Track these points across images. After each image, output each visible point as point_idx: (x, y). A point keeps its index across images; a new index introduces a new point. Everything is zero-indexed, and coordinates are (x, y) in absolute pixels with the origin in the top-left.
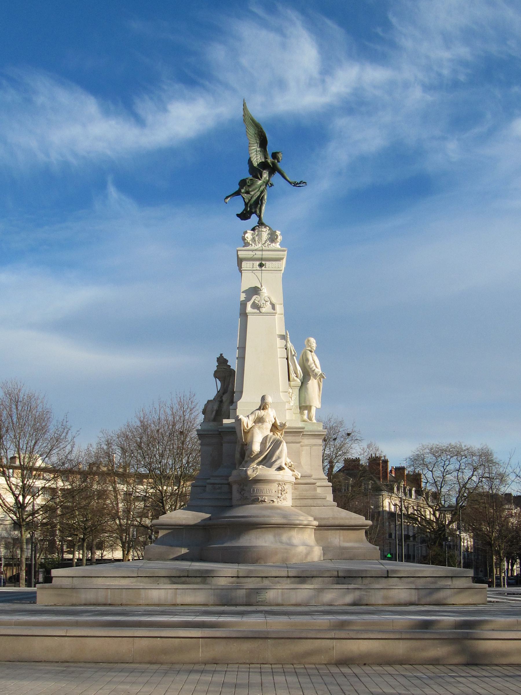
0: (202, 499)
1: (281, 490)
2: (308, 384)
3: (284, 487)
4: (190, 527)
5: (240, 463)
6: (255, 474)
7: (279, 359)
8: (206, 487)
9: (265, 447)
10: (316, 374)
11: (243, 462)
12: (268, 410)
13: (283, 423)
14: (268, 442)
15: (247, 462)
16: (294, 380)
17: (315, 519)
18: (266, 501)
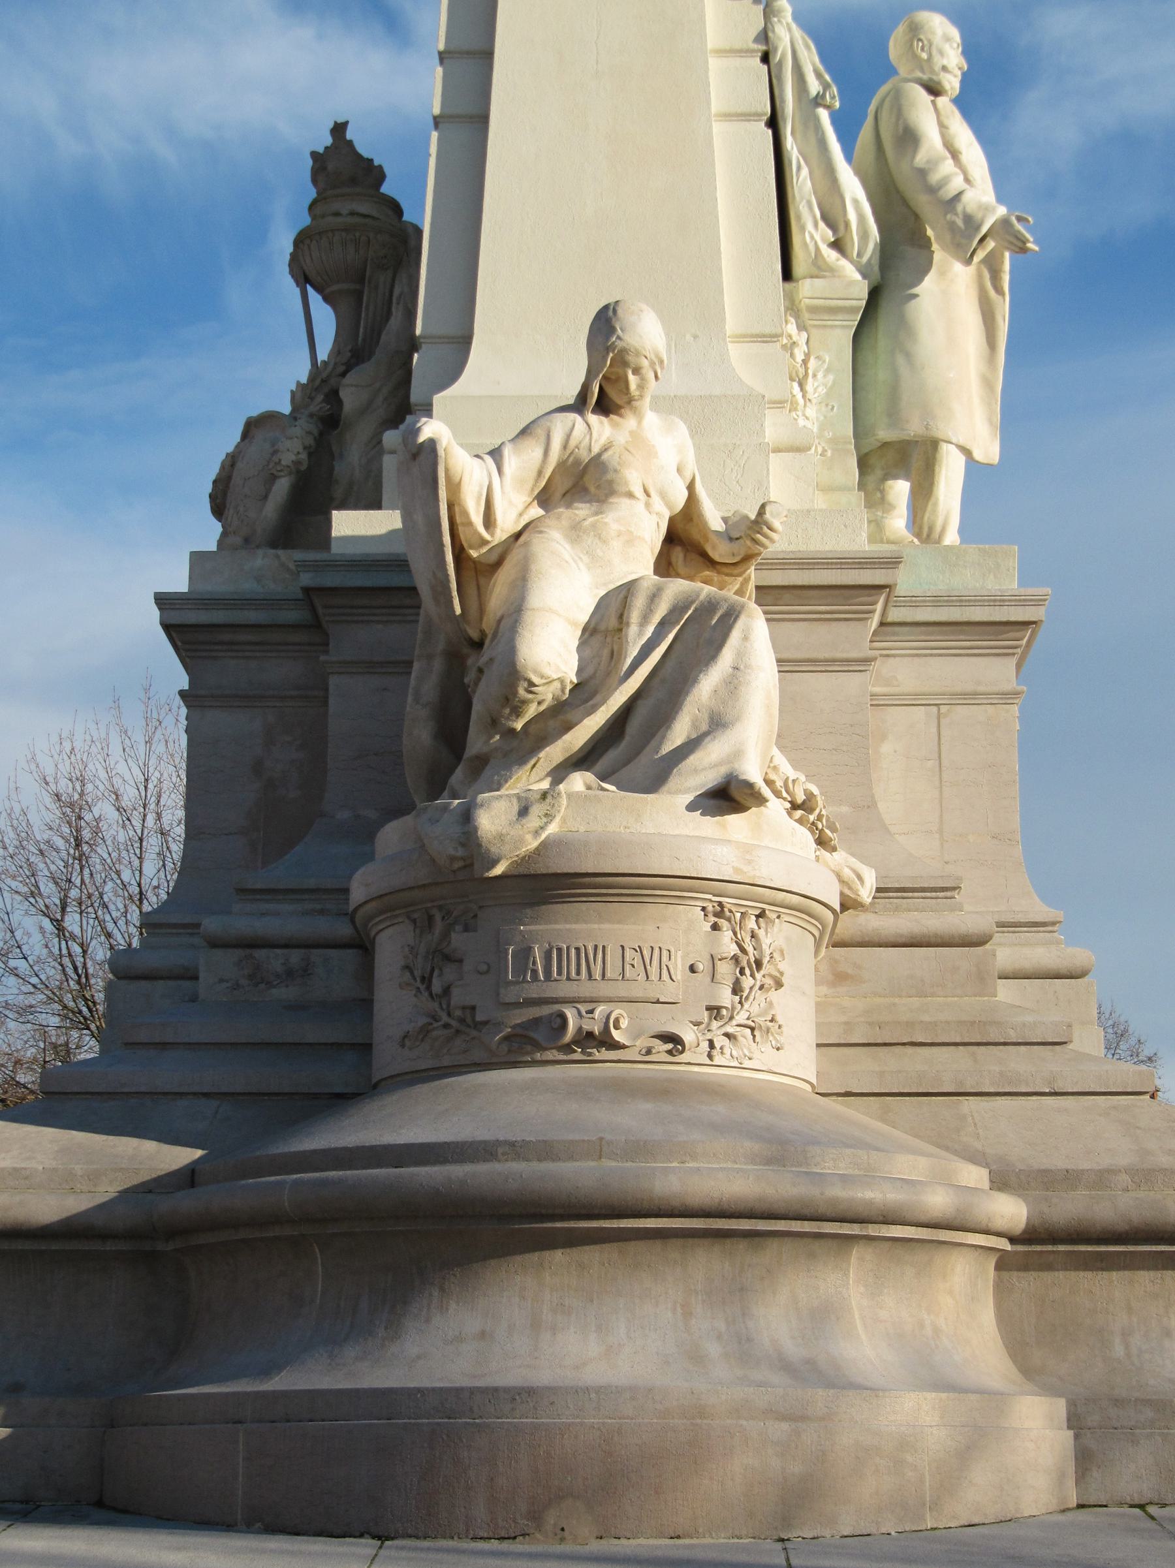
0: (163, 1046)
1: (735, 959)
2: (916, 296)
3: (753, 936)
4: (27, 1245)
5: (437, 785)
6: (537, 833)
7: (717, 128)
8: (196, 978)
9: (615, 656)
10: (971, 223)
11: (459, 773)
12: (640, 418)
13: (747, 517)
14: (635, 616)
15: (481, 763)
16: (820, 269)
17: (1001, 1182)
18: (617, 1035)
